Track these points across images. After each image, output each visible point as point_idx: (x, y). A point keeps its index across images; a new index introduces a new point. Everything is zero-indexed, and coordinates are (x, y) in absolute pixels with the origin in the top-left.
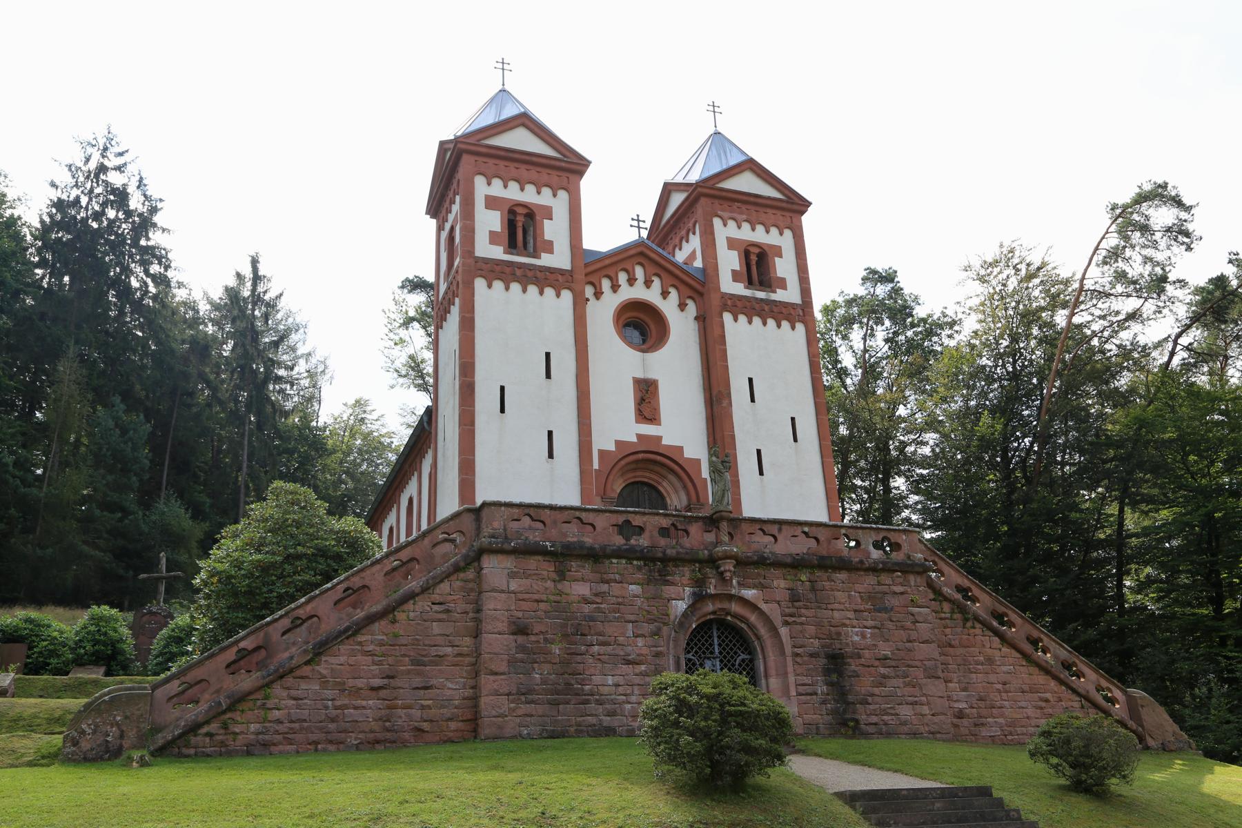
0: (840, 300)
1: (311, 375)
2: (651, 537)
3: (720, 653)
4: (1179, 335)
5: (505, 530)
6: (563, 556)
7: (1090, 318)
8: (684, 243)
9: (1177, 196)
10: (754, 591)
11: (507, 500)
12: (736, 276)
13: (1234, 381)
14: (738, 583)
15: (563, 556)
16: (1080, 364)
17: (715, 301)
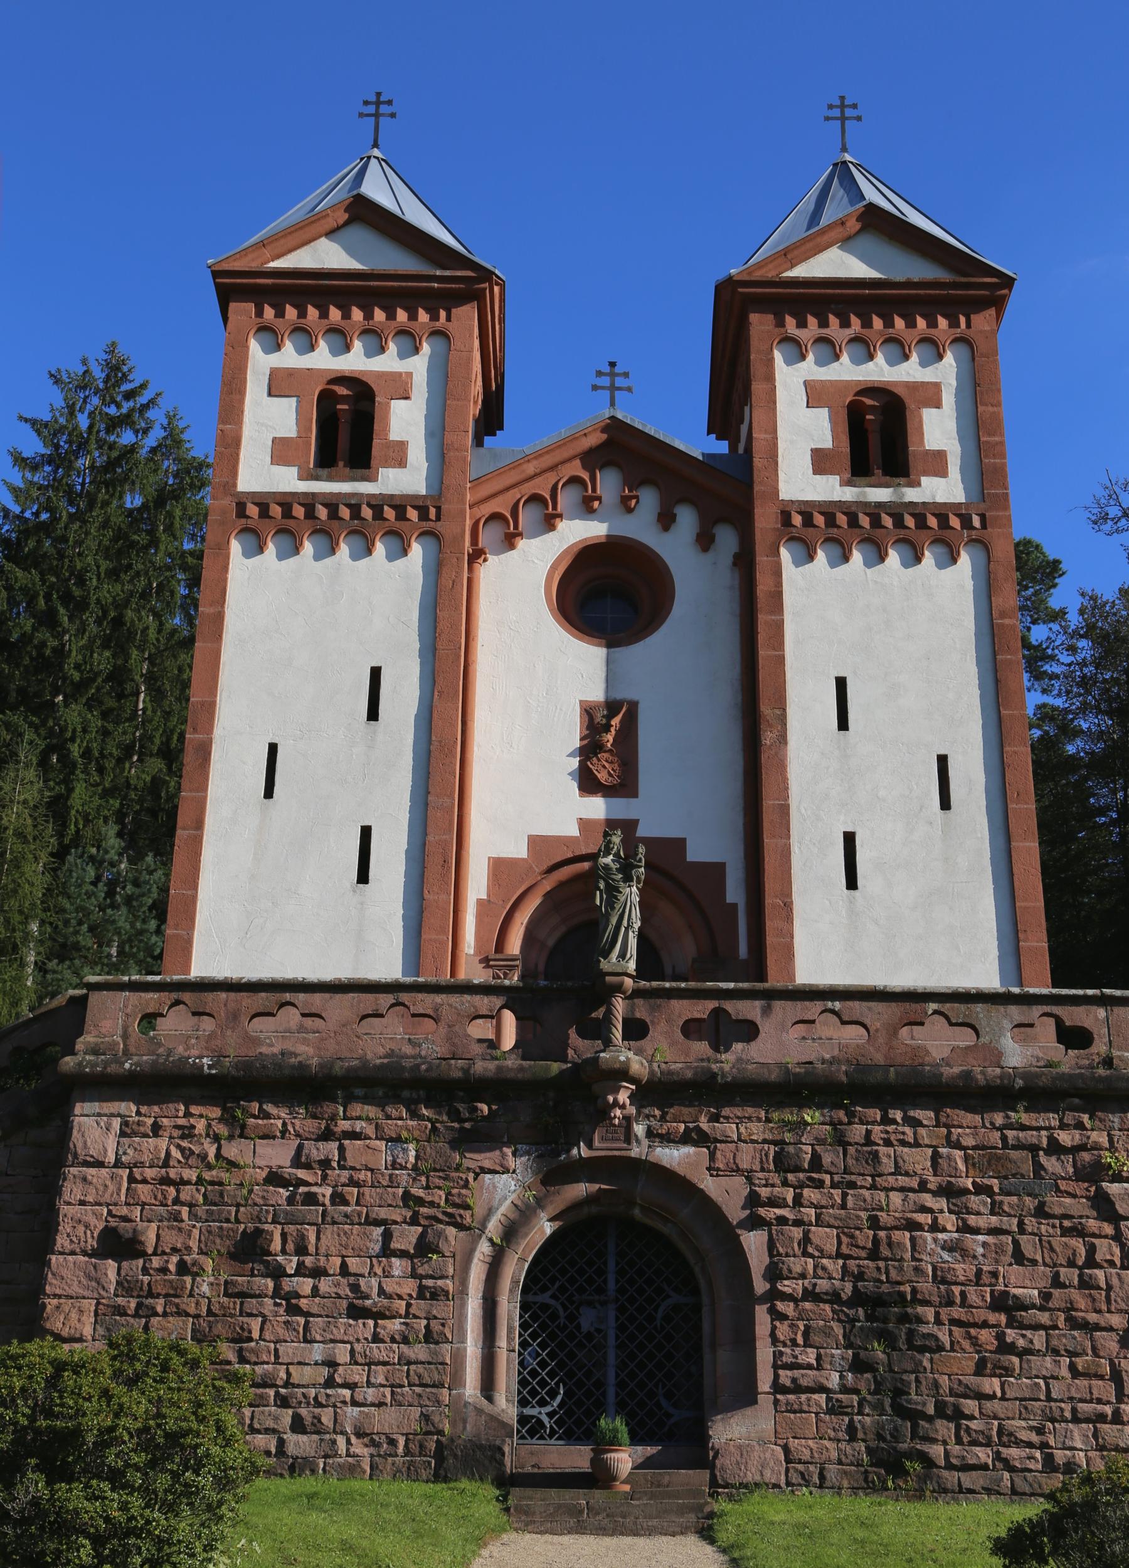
12: (821, 462)
14: (650, 1133)
17: (764, 520)
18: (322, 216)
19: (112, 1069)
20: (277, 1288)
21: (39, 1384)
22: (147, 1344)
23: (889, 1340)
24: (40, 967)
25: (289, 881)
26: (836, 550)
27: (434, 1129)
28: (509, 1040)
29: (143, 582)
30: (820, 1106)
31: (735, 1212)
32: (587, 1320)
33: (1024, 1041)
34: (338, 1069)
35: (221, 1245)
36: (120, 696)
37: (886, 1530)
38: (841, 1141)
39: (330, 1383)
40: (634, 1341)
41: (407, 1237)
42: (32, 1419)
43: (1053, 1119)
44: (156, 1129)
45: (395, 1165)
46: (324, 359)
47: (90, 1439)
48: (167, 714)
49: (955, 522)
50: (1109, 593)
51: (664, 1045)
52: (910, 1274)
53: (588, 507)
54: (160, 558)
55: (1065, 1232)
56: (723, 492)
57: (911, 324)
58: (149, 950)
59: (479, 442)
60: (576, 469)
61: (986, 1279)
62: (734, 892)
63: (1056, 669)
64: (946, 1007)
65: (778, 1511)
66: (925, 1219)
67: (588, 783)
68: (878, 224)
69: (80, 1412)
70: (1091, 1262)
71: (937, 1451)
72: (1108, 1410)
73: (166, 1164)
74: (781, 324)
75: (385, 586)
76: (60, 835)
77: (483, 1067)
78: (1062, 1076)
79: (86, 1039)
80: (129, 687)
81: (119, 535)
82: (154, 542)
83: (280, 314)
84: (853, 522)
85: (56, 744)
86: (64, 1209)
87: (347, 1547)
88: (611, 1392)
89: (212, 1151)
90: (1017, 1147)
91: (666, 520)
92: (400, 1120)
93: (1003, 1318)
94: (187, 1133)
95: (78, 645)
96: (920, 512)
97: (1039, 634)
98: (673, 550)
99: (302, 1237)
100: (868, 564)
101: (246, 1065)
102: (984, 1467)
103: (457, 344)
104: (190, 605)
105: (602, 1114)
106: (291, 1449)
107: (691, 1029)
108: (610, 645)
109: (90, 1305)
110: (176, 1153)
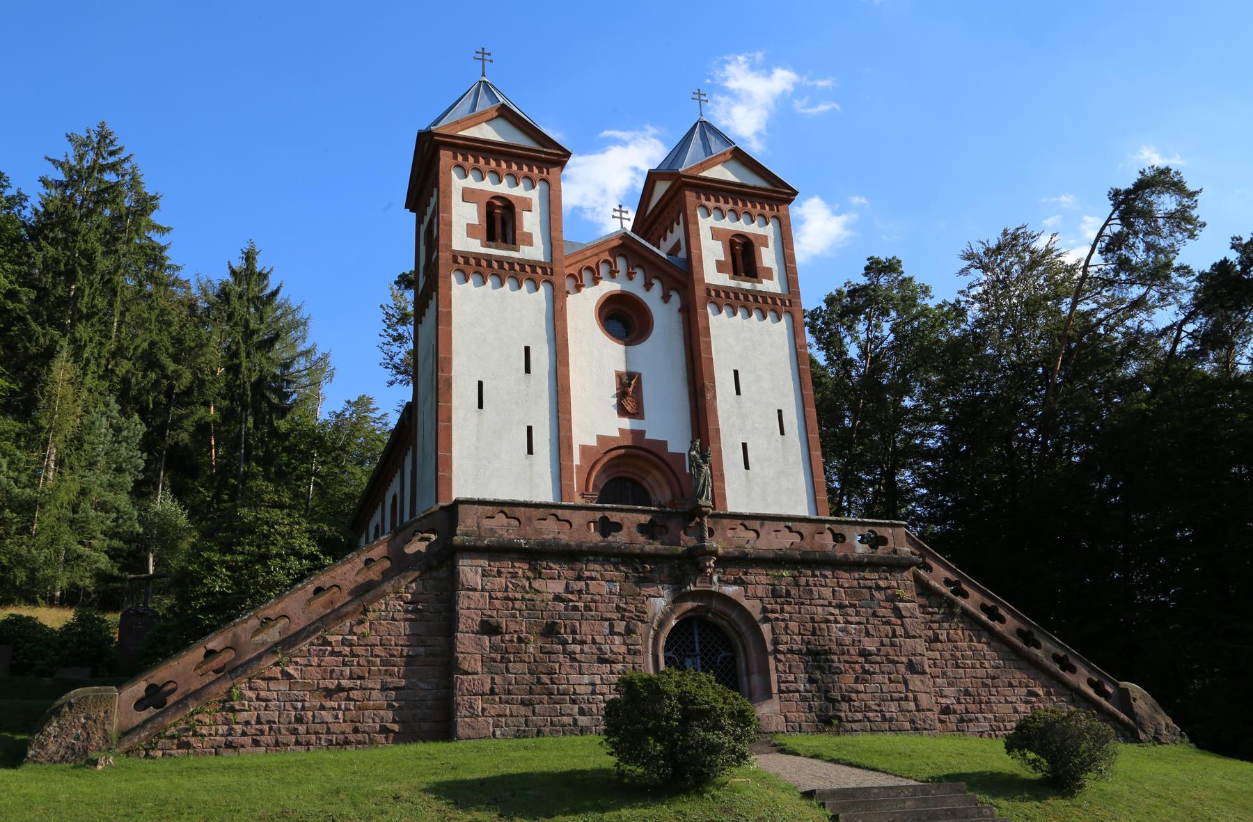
0: (846, 290)
1: (310, 371)
2: (629, 534)
3: (701, 650)
4: (1184, 322)
5: (479, 527)
6: (537, 555)
7: (1095, 306)
8: (668, 233)
9: (1180, 181)
10: (736, 588)
11: (481, 497)
13: (1243, 367)
14: (719, 580)
15: (537, 555)
16: (1084, 351)
17: (700, 293)
19: (479, 543)
23: (822, 670)
27: (627, 577)
31: (757, 616)
34: (585, 547)
35: (536, 629)
38: (797, 584)
39: (593, 693)
41: (620, 627)
44: (499, 573)
45: (611, 593)
52: (827, 642)
53: (613, 274)
55: (884, 623)
56: (678, 276)
60: (606, 256)
66: (832, 618)
67: (622, 411)
68: (505, 114)
70: (894, 636)
73: (506, 591)
79: (460, 529)
90: (865, 587)
91: (648, 286)
92: (612, 573)
94: (514, 575)
96: (523, 264)
99: (574, 626)
106: (580, 723)
108: (626, 344)
109: (478, 657)
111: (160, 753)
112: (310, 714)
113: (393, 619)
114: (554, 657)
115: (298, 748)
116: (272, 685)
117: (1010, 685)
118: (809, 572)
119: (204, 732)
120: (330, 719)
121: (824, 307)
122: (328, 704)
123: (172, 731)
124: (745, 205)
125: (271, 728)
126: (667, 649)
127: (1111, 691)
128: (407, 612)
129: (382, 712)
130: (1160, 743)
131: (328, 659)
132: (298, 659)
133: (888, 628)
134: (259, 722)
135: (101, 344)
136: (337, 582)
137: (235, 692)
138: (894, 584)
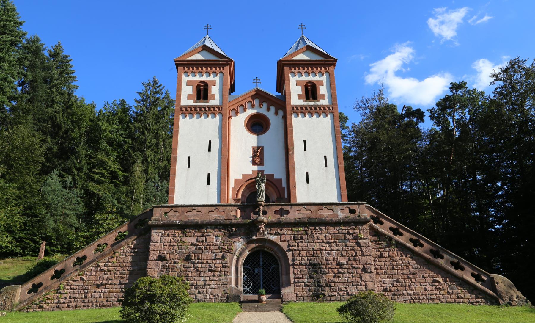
3: (263, 265)
12: (300, 97)
14: (268, 233)
17: (288, 109)
18: (197, 49)
19: (159, 223)
20: (194, 266)
21: (147, 286)
22: (168, 277)
23: (316, 272)
24: (144, 204)
25: (193, 185)
26: (303, 115)
28: (239, 216)
29: (162, 125)
30: (302, 227)
31: (285, 248)
32: (256, 271)
33: (343, 212)
34: (205, 222)
35: (183, 258)
36: (158, 148)
37: (316, 308)
38: (307, 234)
39: (205, 284)
40: (266, 274)
41: (220, 256)
42: (146, 292)
43: (348, 228)
45: (217, 241)
46: (198, 78)
47: (158, 296)
48: (167, 152)
49: (327, 109)
50: (357, 123)
51: (271, 216)
52: (320, 259)
53: (252, 107)
54: (165, 120)
55: (351, 250)
56: (280, 103)
57: (317, 69)
58: (165, 200)
59: (230, 94)
60: (250, 99)
61: (335, 259)
62: (284, 185)
63: (348, 138)
64: (327, 206)
65: (295, 306)
67: (254, 163)
69: (156, 291)
70: (356, 255)
71: (326, 293)
72: (359, 283)
73: (170, 242)
74: (291, 69)
75: (210, 125)
76: (147, 177)
77: (234, 221)
78: (350, 219)
80: (159, 147)
81: (157, 116)
82: (164, 117)
83: (189, 69)
84: (306, 109)
85: (145, 159)
86: (150, 251)
87: (210, 316)
88: (262, 284)
89: (180, 239)
91: (268, 109)
92: (217, 232)
93: (339, 267)
94: (174, 236)
95: (149, 138)
96: (320, 107)
97: (344, 131)
98: (269, 114)
99: (199, 256)
100: (310, 117)
101: (186, 222)
102: (335, 296)
103: (225, 74)
104: (171, 130)
105: (259, 230)
106: (198, 297)
107: (276, 212)
110: (172, 240)
111: (32, 310)
112: (90, 295)
113: (126, 256)
114: (189, 269)
115: (84, 308)
116: (77, 283)
117: (423, 277)
118: (313, 228)
119: (49, 302)
120: (98, 296)
121: (436, 108)
122: (97, 290)
123: (37, 302)
124: (312, 69)
125: (74, 300)
126: (245, 264)
127: (485, 279)
128: (131, 252)
129: (118, 293)
130: (511, 305)
131: (98, 272)
132: (87, 273)
133: (353, 252)
134: (70, 298)
135: (155, 156)
136: (106, 242)
137: (62, 287)
138: (358, 231)
